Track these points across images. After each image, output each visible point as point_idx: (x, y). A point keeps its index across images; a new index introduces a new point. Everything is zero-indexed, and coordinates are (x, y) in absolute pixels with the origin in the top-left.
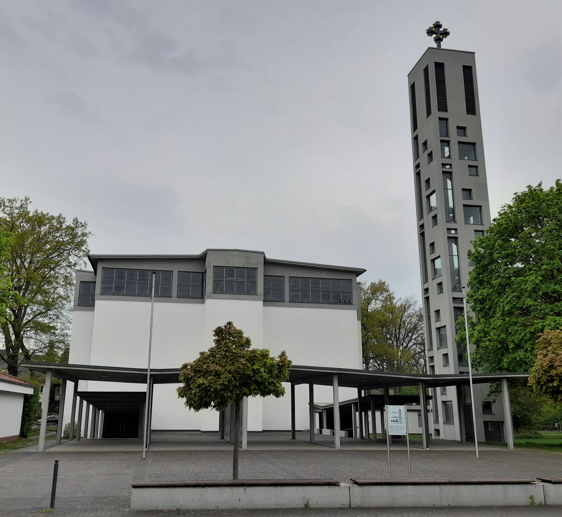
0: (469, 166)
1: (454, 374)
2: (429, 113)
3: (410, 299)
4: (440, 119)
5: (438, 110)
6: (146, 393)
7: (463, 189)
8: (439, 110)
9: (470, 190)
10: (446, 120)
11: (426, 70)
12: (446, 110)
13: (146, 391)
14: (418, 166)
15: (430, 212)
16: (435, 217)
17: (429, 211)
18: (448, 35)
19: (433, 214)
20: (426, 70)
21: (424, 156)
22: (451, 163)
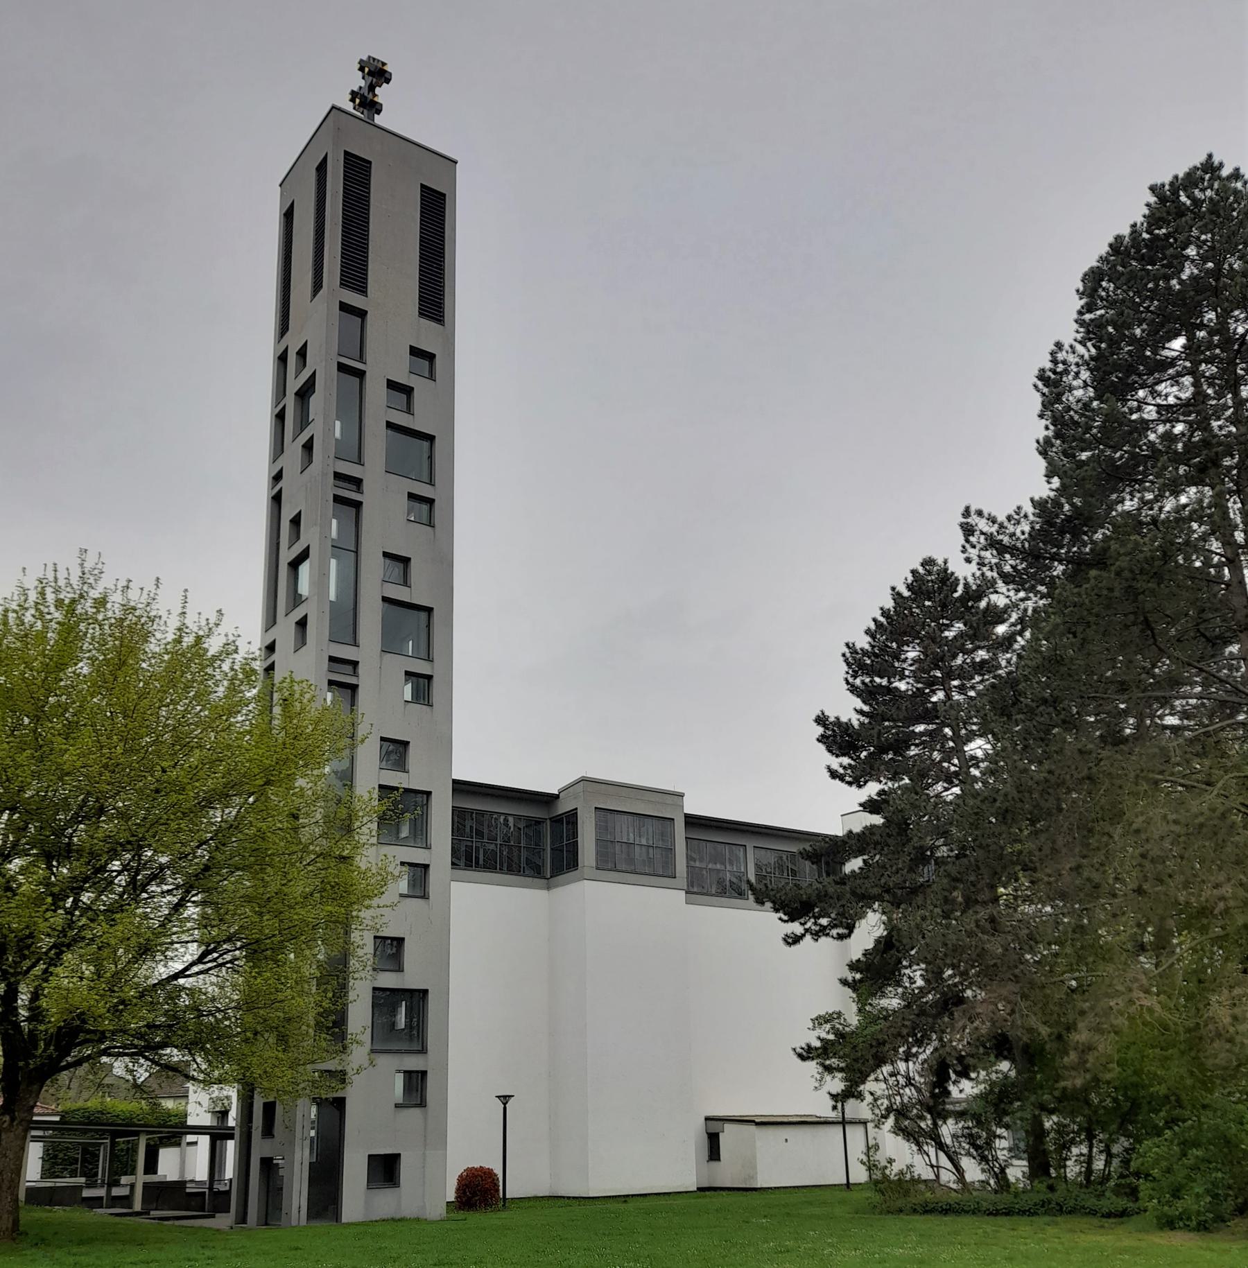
0: (412, 496)
1: (209, 1124)
2: (317, 286)
3: (356, 976)
4: (344, 307)
5: (341, 284)
6: (155, 1173)
7: (386, 555)
8: (343, 284)
9: (405, 561)
10: (362, 314)
11: (322, 168)
12: (362, 290)
13: (160, 1172)
14: (278, 477)
15: (295, 606)
16: (302, 624)
17: (292, 604)
18: (388, 81)
19: (297, 614)
20: (322, 168)
21: (294, 449)
22: (429, 673)
